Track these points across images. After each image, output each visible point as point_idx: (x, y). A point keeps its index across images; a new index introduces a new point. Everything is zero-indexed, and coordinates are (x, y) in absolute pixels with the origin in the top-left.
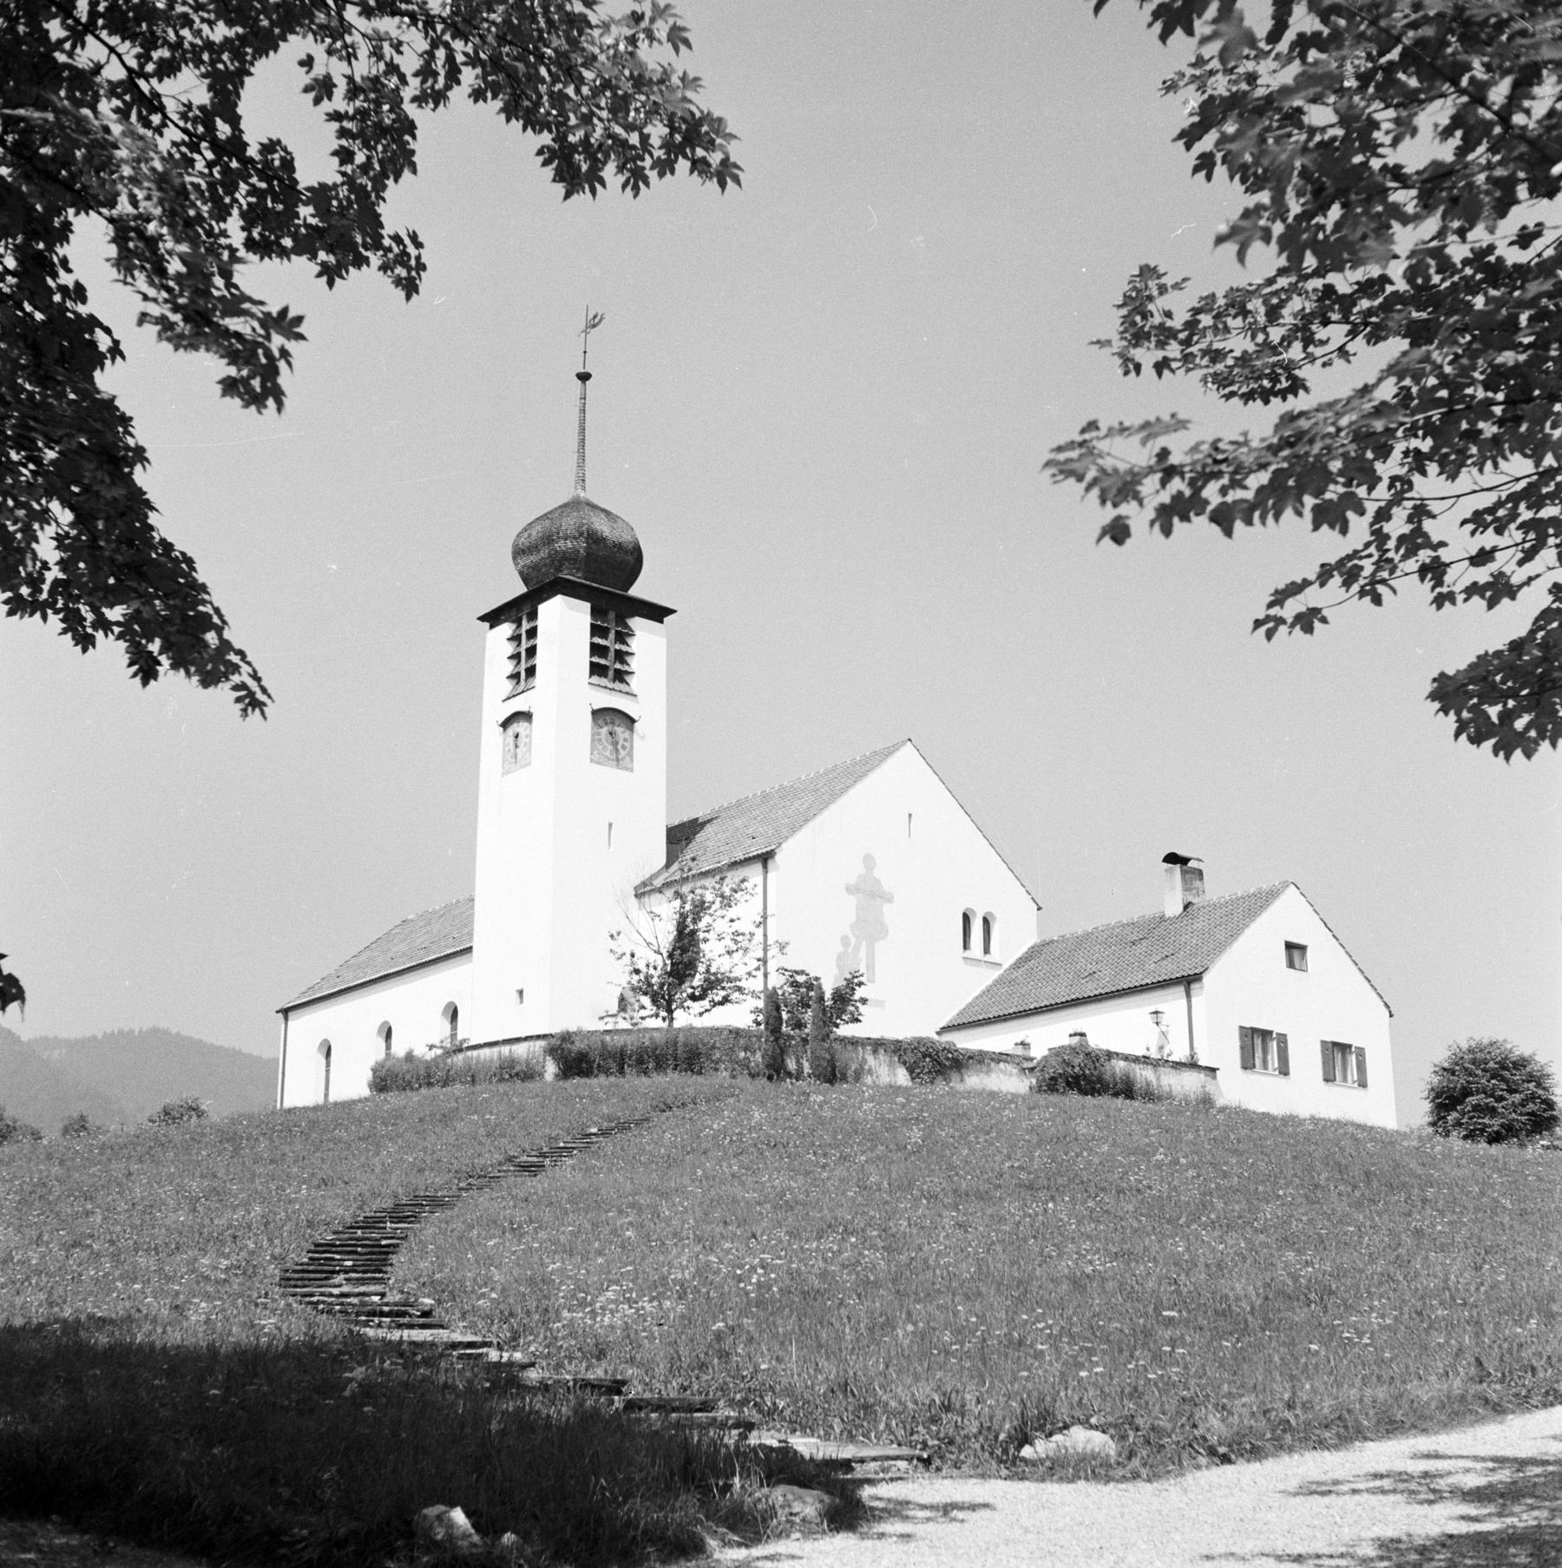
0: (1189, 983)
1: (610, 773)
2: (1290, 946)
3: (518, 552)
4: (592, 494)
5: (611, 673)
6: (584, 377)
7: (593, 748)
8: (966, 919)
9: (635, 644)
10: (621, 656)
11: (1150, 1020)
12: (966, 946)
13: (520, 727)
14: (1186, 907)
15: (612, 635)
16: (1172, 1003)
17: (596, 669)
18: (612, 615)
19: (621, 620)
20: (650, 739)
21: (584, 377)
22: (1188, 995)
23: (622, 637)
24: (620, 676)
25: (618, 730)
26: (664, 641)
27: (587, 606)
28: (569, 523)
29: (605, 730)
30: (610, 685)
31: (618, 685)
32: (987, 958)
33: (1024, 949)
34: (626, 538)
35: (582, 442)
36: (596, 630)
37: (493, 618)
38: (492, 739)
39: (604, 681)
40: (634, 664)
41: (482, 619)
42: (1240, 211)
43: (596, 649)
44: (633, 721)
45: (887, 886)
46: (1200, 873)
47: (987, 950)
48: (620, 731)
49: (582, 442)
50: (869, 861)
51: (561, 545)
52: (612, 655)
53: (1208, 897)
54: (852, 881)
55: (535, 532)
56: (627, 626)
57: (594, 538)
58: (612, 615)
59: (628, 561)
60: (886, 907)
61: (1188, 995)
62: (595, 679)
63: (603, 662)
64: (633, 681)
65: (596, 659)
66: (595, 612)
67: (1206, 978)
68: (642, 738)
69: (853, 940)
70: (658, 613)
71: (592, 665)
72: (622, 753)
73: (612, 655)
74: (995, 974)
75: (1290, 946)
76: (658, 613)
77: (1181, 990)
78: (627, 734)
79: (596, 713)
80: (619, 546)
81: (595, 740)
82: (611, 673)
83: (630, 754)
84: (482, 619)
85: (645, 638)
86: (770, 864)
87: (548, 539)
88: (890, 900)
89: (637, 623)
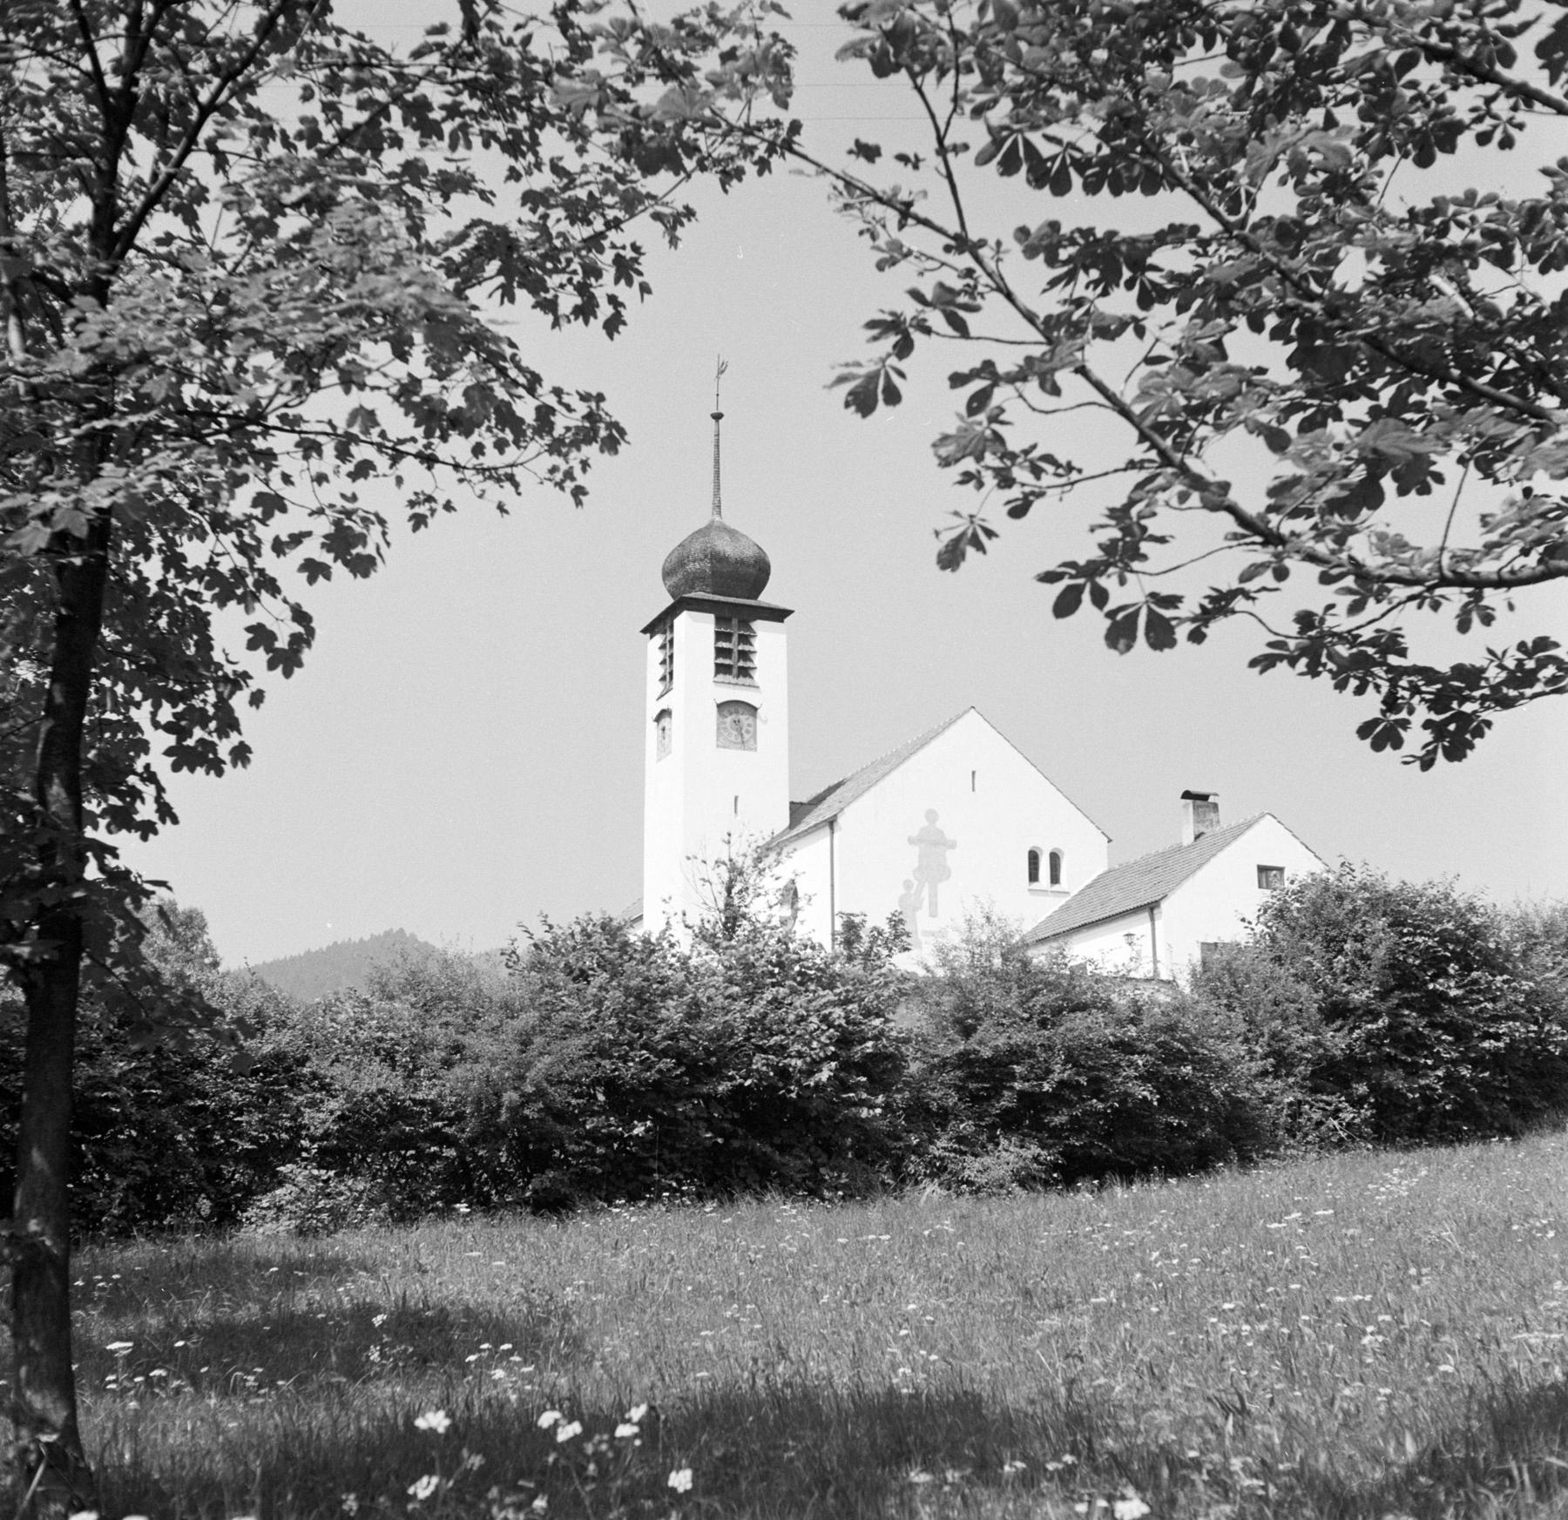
0: (1152, 910)
1: (735, 755)
2: (1263, 870)
3: (667, 574)
4: (729, 519)
5: (735, 671)
6: (717, 417)
7: (719, 734)
8: (1034, 858)
9: (757, 644)
10: (745, 655)
11: (1123, 941)
12: (1033, 876)
13: (665, 722)
14: (1197, 837)
15: (735, 639)
16: (1140, 926)
17: (721, 669)
18: (735, 622)
19: (745, 624)
20: (772, 725)
21: (717, 417)
22: (1152, 919)
23: (745, 639)
24: (745, 672)
25: (743, 718)
26: (784, 637)
27: (712, 617)
28: (696, 547)
29: (729, 720)
30: (734, 680)
31: (742, 680)
32: (1056, 887)
33: (1094, 877)
34: (749, 553)
35: (717, 474)
36: (719, 636)
37: (651, 629)
38: (652, 728)
39: (728, 678)
40: (757, 660)
41: (644, 631)
42: (898, 266)
43: (720, 652)
44: (756, 709)
45: (949, 836)
46: (1215, 806)
47: (1055, 879)
48: (745, 719)
49: (717, 474)
50: (931, 815)
51: (691, 567)
52: (735, 655)
53: (1224, 825)
54: (915, 833)
55: (674, 560)
56: (750, 629)
57: (717, 558)
58: (735, 622)
59: (756, 573)
60: (949, 854)
61: (1152, 919)
62: (721, 677)
63: (727, 662)
64: (756, 675)
65: (721, 661)
66: (719, 621)
67: (1164, 905)
68: (765, 722)
69: (916, 883)
70: (779, 615)
71: (717, 665)
72: (746, 736)
73: (735, 655)
74: (1063, 901)
75: (1263, 870)
76: (779, 615)
77: (1146, 915)
78: (751, 720)
79: (719, 706)
80: (741, 562)
81: (720, 729)
82: (735, 671)
83: (754, 736)
84: (644, 631)
85: (765, 635)
86: (836, 827)
87: (681, 563)
88: (953, 846)
89: (759, 626)
